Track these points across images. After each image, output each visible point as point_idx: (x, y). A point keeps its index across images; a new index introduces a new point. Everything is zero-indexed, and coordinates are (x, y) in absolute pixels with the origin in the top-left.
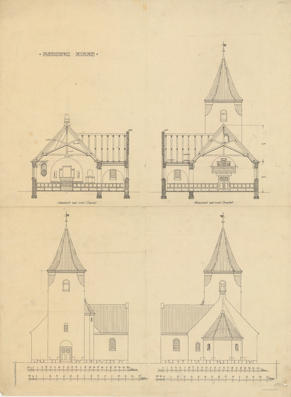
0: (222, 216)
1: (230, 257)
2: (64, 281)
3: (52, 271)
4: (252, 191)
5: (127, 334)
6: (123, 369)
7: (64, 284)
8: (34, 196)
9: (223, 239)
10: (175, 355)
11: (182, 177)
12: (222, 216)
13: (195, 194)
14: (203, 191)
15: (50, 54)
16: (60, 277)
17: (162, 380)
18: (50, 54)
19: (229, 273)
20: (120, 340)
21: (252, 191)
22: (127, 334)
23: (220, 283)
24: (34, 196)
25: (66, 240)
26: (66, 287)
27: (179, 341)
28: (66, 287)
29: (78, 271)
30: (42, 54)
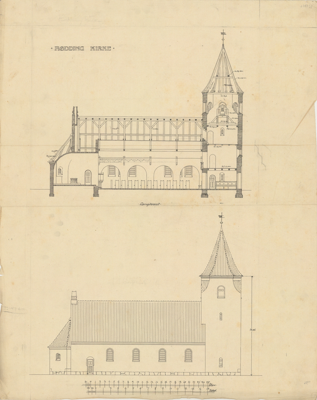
0: (221, 217)
1: (229, 262)
2: (219, 287)
3: (206, 277)
4: (234, 189)
5: (204, 344)
6: (202, 384)
7: (218, 290)
8: (52, 194)
9: (221, 244)
10: (136, 367)
11: (137, 173)
12: (221, 217)
13: (100, 191)
14: (230, 189)
15: (62, 49)
16: (214, 283)
17: (94, 392)
18: (62, 49)
19: (227, 277)
20: (197, 350)
21: (234, 189)
22: (204, 344)
23: (218, 288)
24: (52, 194)
25: (221, 244)
26: (221, 294)
27: (165, 351)
28: (221, 293)
29: (234, 276)
30: (54, 48)
